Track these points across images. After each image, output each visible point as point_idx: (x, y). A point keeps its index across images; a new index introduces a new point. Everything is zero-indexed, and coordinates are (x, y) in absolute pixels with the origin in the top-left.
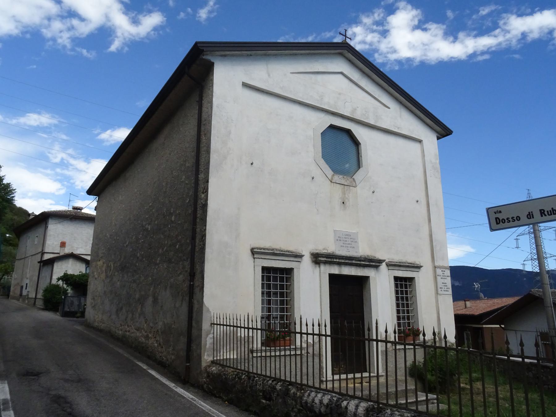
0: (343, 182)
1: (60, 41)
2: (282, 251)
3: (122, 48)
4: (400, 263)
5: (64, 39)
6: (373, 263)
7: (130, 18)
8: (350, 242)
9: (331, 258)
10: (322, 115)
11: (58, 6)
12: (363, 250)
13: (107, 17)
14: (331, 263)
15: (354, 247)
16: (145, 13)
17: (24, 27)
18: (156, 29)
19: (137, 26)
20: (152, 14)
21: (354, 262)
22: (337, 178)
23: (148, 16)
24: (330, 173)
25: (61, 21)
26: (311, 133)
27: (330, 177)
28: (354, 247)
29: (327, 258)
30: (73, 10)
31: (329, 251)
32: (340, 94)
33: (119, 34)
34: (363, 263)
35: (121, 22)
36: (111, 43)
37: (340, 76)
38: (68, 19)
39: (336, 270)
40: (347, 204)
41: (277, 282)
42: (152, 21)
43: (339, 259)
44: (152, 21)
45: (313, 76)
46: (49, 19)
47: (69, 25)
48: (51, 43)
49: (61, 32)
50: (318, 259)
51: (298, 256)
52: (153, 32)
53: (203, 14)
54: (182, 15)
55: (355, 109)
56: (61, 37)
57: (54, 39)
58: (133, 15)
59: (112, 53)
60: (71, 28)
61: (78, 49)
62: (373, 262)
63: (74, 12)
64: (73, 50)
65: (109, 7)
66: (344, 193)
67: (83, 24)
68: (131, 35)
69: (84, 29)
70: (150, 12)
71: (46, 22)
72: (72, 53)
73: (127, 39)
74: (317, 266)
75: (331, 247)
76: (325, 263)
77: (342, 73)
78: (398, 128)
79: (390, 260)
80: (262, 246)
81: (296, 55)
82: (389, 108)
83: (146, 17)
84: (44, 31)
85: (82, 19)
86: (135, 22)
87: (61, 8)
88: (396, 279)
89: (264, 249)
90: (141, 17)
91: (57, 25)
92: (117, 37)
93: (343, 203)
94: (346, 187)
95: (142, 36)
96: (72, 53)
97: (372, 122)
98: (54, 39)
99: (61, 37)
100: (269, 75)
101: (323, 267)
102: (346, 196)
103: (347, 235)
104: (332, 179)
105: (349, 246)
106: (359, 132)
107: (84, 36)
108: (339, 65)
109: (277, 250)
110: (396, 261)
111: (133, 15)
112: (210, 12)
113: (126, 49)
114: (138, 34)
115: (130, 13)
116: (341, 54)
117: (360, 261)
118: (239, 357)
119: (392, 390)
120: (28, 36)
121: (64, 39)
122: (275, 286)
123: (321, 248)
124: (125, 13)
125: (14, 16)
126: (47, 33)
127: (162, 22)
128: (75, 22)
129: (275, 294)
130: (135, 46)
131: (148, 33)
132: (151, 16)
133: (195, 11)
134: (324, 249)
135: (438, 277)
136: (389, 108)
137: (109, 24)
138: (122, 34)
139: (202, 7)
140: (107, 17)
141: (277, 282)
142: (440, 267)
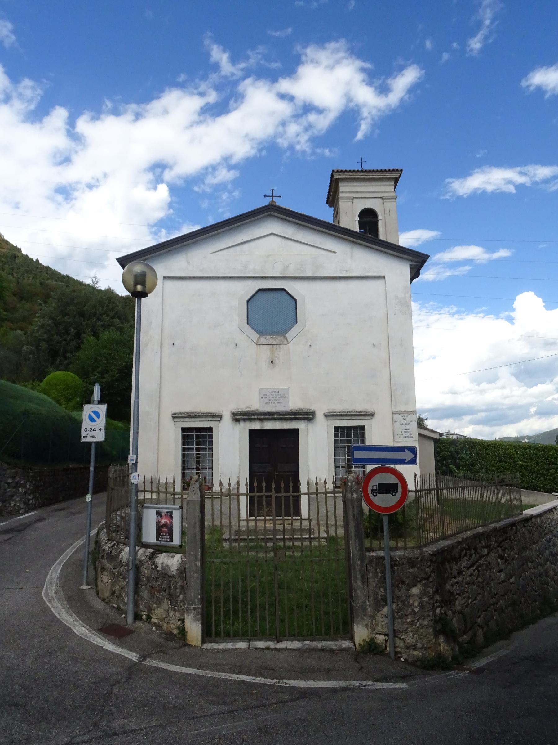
0: (271, 342)
1: (298, 147)
2: (202, 413)
3: (372, 132)
4: (344, 412)
5: (303, 144)
6: (308, 416)
7: (376, 88)
8: (277, 398)
9: (248, 415)
10: (249, 283)
11: (292, 104)
12: (294, 403)
13: (349, 98)
14: (250, 420)
15: (282, 403)
16: (395, 73)
17: (260, 143)
18: (412, 90)
19: (386, 95)
20: (404, 72)
21: (275, 417)
22: (263, 340)
23: (399, 76)
24: (255, 336)
25: (296, 122)
26: (236, 303)
27: (255, 340)
28: (282, 403)
29: (243, 415)
30: (307, 104)
31: (253, 409)
32: (268, 256)
33: (365, 113)
34: (288, 417)
35: (366, 95)
36: (356, 129)
37: (272, 237)
38: (304, 116)
39: (257, 425)
40: (277, 361)
41: (197, 440)
42: (405, 80)
43: (258, 415)
44: (405, 80)
45: (238, 248)
46: (283, 124)
47: (305, 124)
48: (288, 153)
49: (297, 135)
50: (239, 417)
51: (218, 417)
52: (407, 96)
53: (476, 44)
54: (445, 56)
55: (287, 267)
56: (299, 142)
57: (291, 147)
58: (380, 81)
59: (360, 141)
60: (309, 127)
61: (318, 150)
62: (300, 415)
63: (309, 105)
64: (314, 153)
65: (348, 83)
66: (273, 352)
67: (321, 116)
68: (380, 110)
69: (322, 123)
70: (401, 69)
71: (281, 129)
72: (313, 158)
73: (376, 118)
74: (238, 423)
75: (255, 404)
76: (244, 420)
77: (272, 234)
78: (347, 271)
79: (330, 411)
80: (183, 411)
81: (217, 234)
82: (336, 253)
83: (397, 79)
84: (280, 141)
85: (320, 111)
86: (383, 90)
87: (295, 104)
88: (336, 428)
89: (184, 413)
90: (389, 81)
91: (293, 128)
92: (363, 119)
93: (272, 362)
94: (275, 346)
95: (393, 107)
96: (313, 158)
97: (309, 274)
98: (291, 147)
99: (299, 142)
100: (188, 263)
101: (242, 424)
102: (276, 355)
103: (276, 392)
104: (258, 341)
105: (276, 402)
106: (292, 287)
107: (324, 132)
108: (274, 226)
109: (196, 413)
110: (338, 411)
111: (380, 81)
112: (486, 38)
113: (377, 131)
114: (388, 106)
115: (375, 80)
116: (270, 215)
117: (283, 415)
118: (314, 516)
119: (226, 522)
120: (264, 153)
121: (303, 144)
122: (343, 442)
123: (243, 407)
124: (370, 83)
125: (247, 135)
126: (283, 143)
127: (419, 79)
128: (312, 117)
129: (343, 447)
130: (387, 122)
131: (401, 100)
132: (403, 75)
133: (464, 44)
134: (247, 407)
135: (395, 423)
136: (336, 253)
137: (352, 105)
138: (369, 113)
139: (473, 34)
140: (349, 98)
141: (197, 440)
142: (399, 413)
